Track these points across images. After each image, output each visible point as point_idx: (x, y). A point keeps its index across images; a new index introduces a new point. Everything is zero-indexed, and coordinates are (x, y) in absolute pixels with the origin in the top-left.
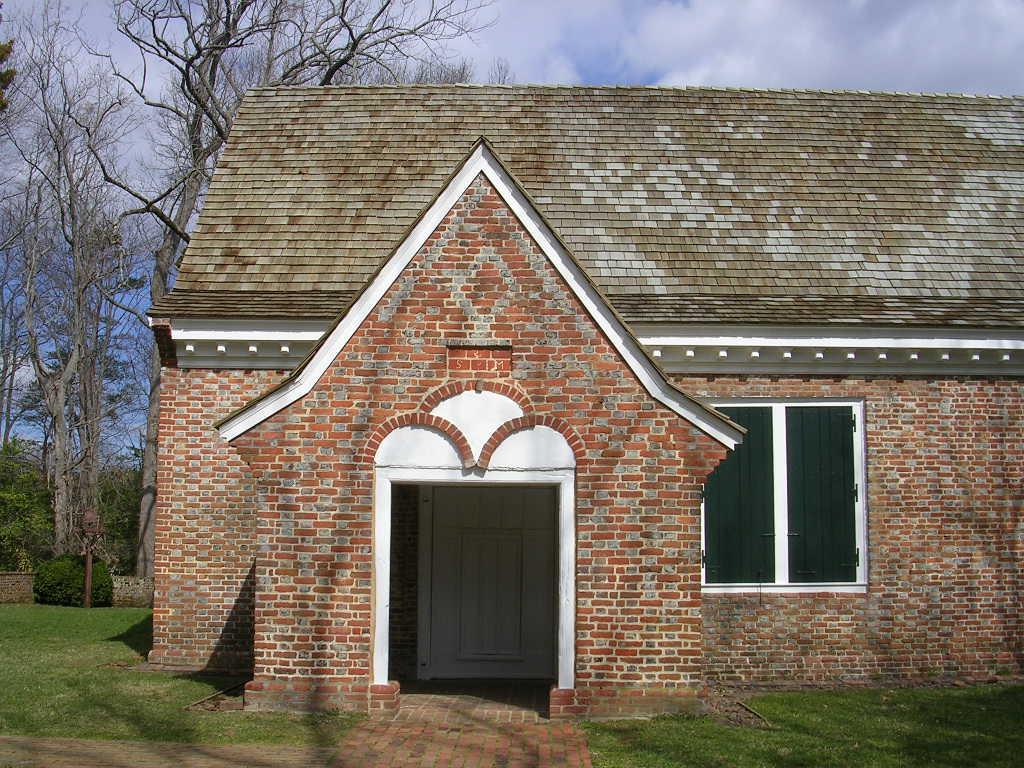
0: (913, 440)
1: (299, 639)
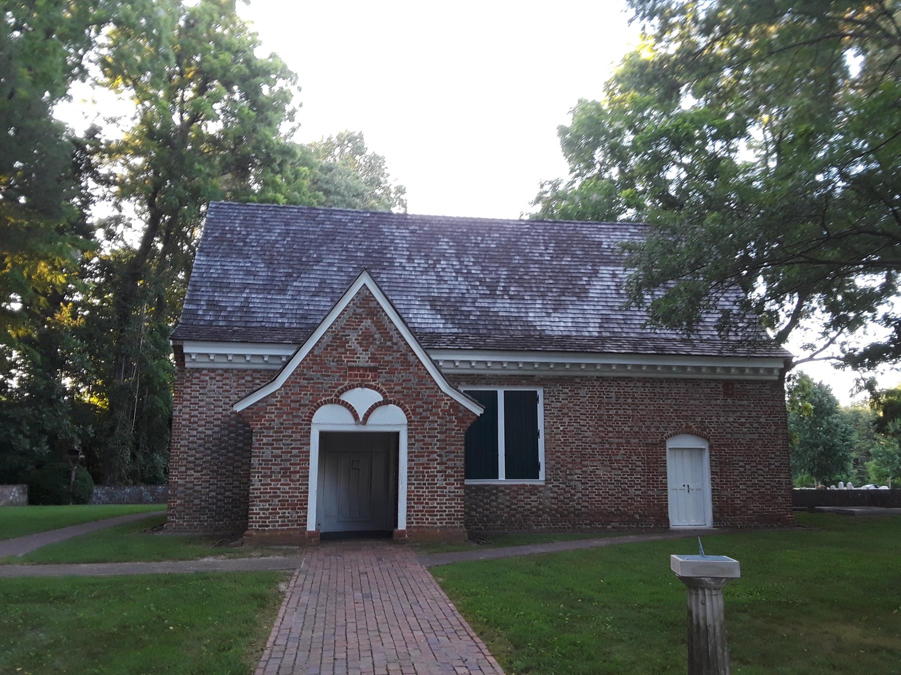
0: (567, 408)
1: (272, 509)
